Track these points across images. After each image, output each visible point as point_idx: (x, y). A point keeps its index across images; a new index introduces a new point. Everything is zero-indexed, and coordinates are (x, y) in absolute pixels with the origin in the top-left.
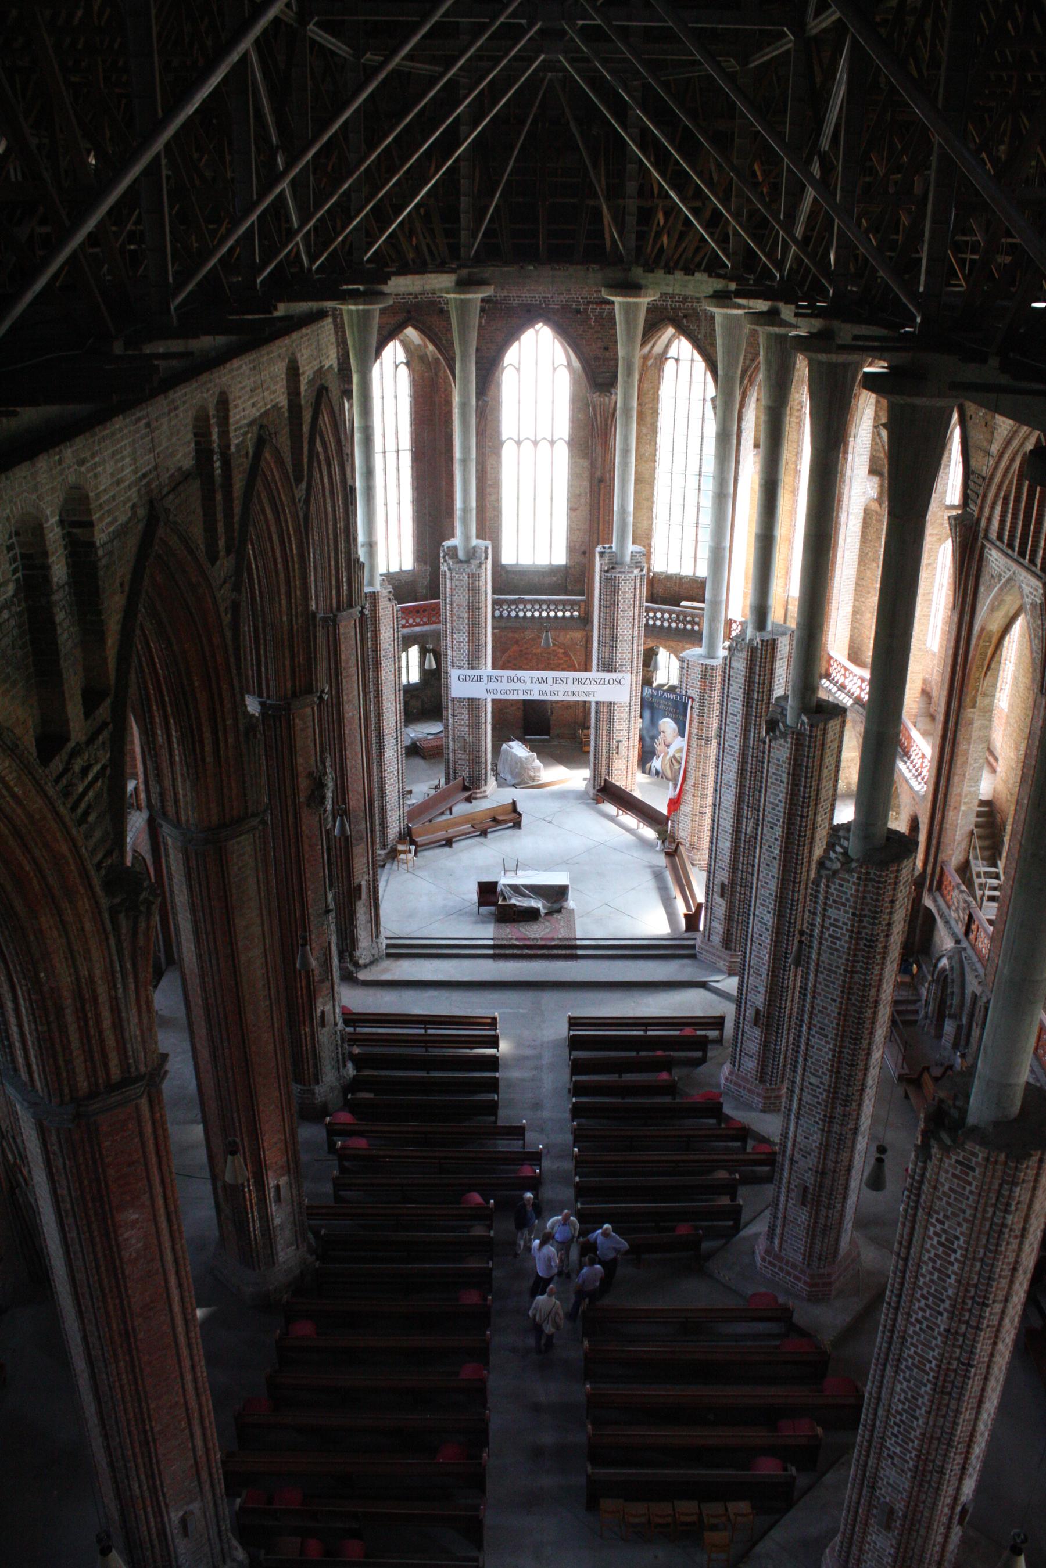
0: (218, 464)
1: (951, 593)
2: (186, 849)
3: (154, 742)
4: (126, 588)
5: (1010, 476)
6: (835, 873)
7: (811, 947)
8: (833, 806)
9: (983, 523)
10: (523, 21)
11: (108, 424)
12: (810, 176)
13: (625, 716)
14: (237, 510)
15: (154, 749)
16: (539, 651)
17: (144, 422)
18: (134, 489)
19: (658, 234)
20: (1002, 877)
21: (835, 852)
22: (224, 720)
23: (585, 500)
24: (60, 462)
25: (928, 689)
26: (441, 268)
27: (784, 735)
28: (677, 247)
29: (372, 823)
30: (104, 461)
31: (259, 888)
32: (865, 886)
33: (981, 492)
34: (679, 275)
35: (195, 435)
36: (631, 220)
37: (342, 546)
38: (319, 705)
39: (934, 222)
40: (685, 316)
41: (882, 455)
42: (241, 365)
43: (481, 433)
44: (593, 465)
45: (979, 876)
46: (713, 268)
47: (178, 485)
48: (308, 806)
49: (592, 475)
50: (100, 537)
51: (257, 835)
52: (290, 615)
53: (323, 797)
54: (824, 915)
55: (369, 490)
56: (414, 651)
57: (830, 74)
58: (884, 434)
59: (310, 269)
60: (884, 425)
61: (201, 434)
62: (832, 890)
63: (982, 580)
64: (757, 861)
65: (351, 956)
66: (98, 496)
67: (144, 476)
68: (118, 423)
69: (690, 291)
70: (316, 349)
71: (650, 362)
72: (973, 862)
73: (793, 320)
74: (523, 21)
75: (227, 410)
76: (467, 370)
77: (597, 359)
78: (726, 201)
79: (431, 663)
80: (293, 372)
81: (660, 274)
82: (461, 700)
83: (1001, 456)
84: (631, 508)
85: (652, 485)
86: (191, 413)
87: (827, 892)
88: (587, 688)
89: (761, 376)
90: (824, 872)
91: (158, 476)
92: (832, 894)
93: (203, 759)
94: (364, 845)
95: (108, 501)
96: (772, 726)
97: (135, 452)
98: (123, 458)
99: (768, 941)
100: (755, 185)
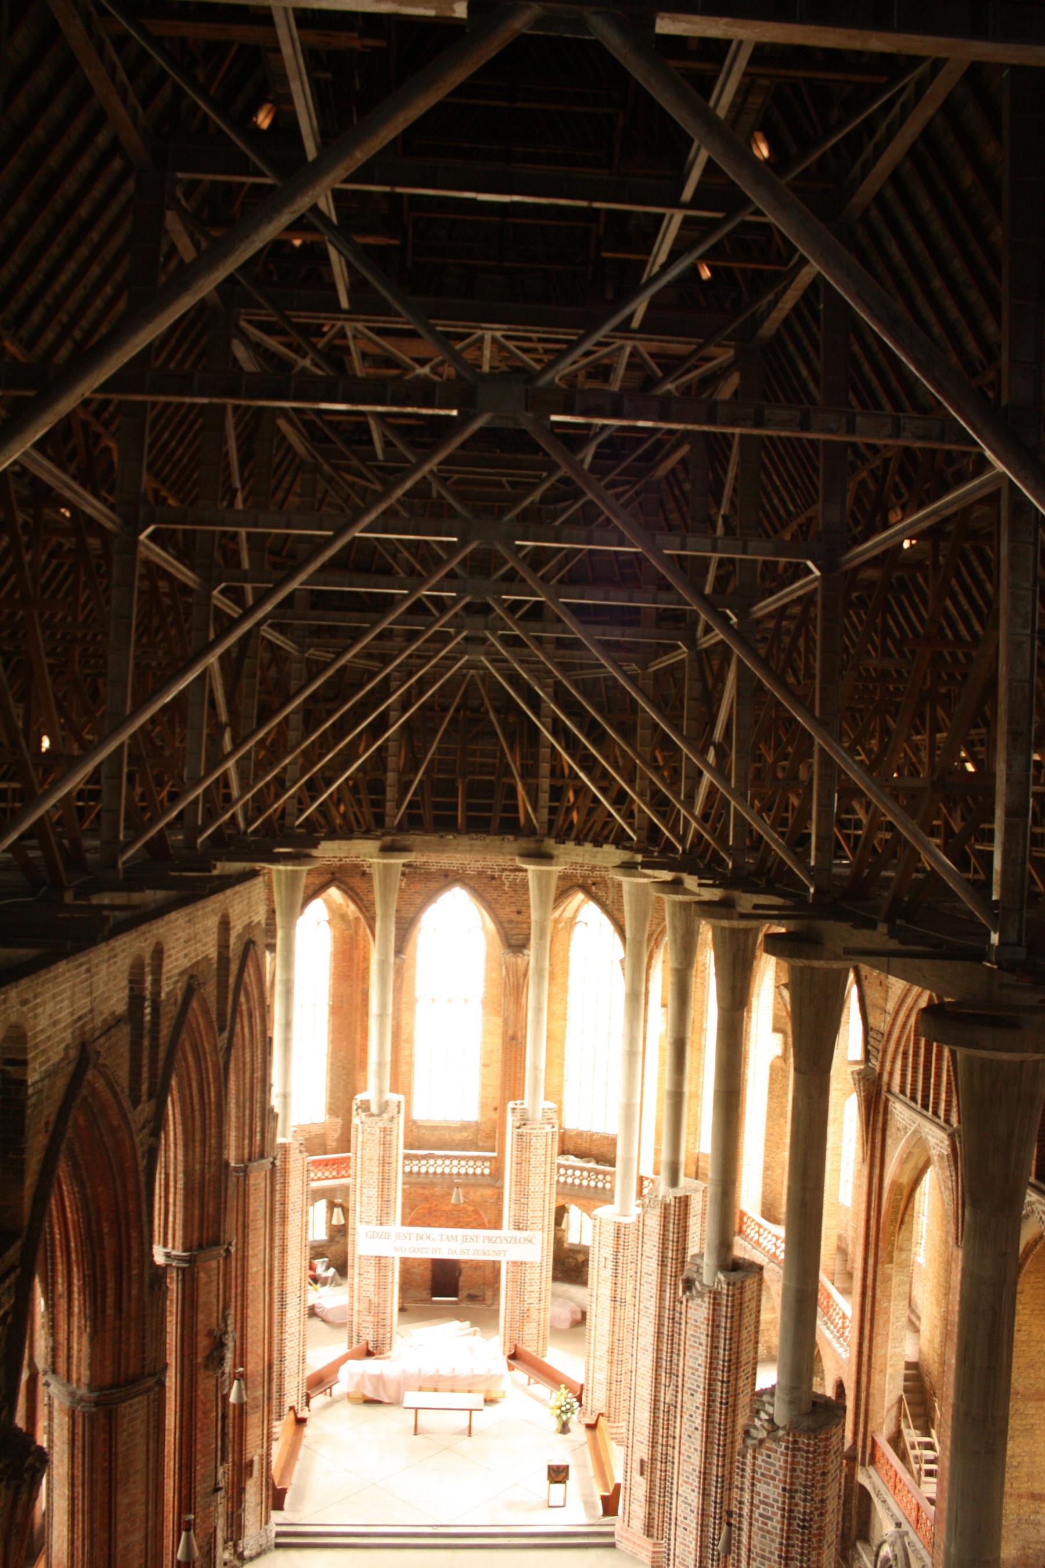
0: (148, 1011)
1: (859, 1147)
2: (73, 1412)
3: (53, 1291)
4: (51, 1128)
5: (907, 1031)
6: (761, 1442)
7: (740, 1529)
8: (754, 1369)
9: (885, 1077)
10: (452, 630)
11: (53, 968)
12: (705, 763)
13: (536, 1276)
14: (162, 1056)
15: (53, 1299)
16: (449, 1208)
17: (84, 967)
18: (69, 1031)
19: (569, 810)
20: (937, 1446)
21: (760, 1419)
22: (130, 1269)
23: (498, 1055)
24: (5, 1001)
25: (843, 1245)
26: (367, 834)
27: (701, 1295)
28: (586, 821)
29: (270, 1390)
30: (44, 1003)
31: (148, 1459)
32: (794, 1456)
33: (880, 1048)
34: (588, 846)
35: (131, 982)
36: (544, 797)
37: (258, 1095)
38: (226, 1258)
39: (819, 805)
40: (594, 884)
41: (784, 1014)
42: (178, 918)
43: (398, 990)
44: (506, 1022)
45: (913, 1447)
46: (620, 840)
47: (109, 1029)
48: (206, 1367)
49: (505, 1033)
50: (33, 1077)
51: (152, 1397)
52: (203, 1163)
53: (222, 1359)
54: (752, 1491)
55: (287, 1041)
56: (322, 1205)
57: (721, 679)
58: (786, 994)
59: (245, 833)
60: (786, 986)
61: (135, 981)
62: (759, 1462)
63: (888, 1133)
64: (678, 1431)
65: (235, 1546)
66: (35, 1036)
67: (80, 1018)
68: (62, 966)
69: (598, 861)
70: (246, 905)
71: (561, 926)
72: (905, 1431)
73: (696, 889)
74: (452, 630)
75: (161, 959)
76: (386, 928)
77: (510, 922)
78: (631, 782)
79: (338, 1218)
80: (225, 925)
81: (570, 845)
82: (368, 1258)
83: (897, 1012)
84: (542, 1065)
85: (562, 1042)
86: (129, 961)
87: (754, 1464)
88: (497, 1247)
89: (667, 939)
90: (750, 1442)
91: (92, 1020)
92: (760, 1467)
93: (104, 1311)
94: (259, 1414)
95: (43, 1042)
96: (689, 1284)
97: (73, 995)
98: (62, 1001)
99: (694, 1525)
100: (657, 769)
